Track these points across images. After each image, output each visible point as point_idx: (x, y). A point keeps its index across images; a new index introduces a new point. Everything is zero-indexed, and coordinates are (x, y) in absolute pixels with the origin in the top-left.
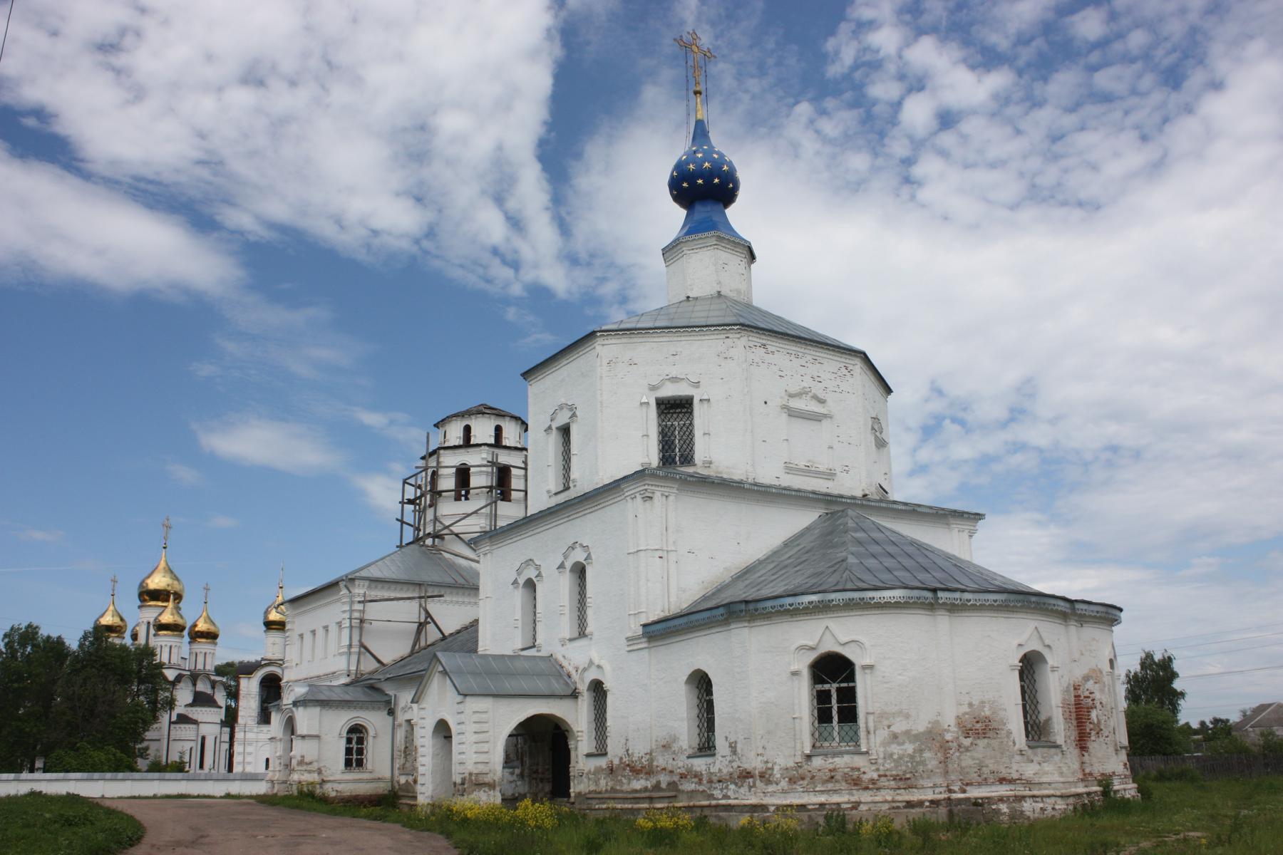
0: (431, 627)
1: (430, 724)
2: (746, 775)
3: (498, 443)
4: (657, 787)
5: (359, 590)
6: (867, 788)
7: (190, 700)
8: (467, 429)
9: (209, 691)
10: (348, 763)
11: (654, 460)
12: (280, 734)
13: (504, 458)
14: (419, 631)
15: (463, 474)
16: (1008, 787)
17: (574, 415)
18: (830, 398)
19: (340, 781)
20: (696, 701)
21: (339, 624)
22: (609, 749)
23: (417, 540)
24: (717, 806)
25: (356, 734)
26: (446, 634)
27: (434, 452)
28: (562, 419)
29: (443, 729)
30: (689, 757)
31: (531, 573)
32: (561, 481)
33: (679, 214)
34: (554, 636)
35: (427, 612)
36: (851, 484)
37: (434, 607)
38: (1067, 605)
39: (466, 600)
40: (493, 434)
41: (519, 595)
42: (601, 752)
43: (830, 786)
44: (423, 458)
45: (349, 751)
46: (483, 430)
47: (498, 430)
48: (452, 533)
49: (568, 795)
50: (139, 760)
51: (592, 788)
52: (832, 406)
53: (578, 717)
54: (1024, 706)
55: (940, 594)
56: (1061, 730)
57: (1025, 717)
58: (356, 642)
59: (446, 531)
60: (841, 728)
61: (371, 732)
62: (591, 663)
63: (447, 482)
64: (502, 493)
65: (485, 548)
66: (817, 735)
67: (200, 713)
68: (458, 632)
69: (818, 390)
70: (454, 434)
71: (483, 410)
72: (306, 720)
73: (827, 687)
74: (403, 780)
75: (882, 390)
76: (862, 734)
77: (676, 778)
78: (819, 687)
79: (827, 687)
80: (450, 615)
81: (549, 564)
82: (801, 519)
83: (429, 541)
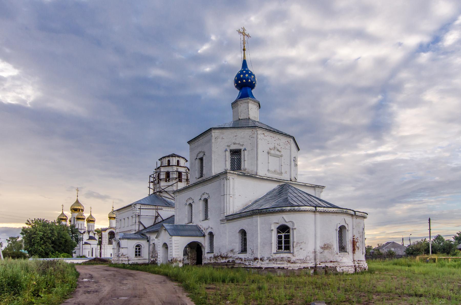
0: (159, 217)
1: (161, 244)
2: (256, 259)
4: (228, 262)
5: (138, 206)
6: (292, 263)
8: (169, 161)
9: (93, 236)
10: (136, 255)
11: (228, 166)
12: (116, 247)
14: (156, 219)
15: (168, 174)
16: (333, 263)
17: (204, 154)
18: (282, 150)
19: (134, 260)
21: (132, 216)
22: (214, 251)
23: (154, 193)
24: (247, 267)
25: (138, 247)
26: (146, 227)
28: (201, 155)
29: (165, 246)
30: (239, 253)
31: (191, 201)
32: (200, 175)
34: (198, 220)
35: (158, 213)
36: (286, 177)
37: (160, 212)
39: (168, 209)
41: (187, 208)
42: (212, 252)
43: (281, 262)
44: (156, 169)
45: (136, 252)
46: (174, 161)
47: (178, 161)
48: (165, 191)
49: (202, 264)
50: (74, 254)
51: (209, 262)
52: (282, 153)
56: (349, 247)
61: (143, 246)
62: (209, 227)
63: (163, 176)
64: (179, 180)
65: (177, 194)
67: (91, 242)
68: (168, 219)
69: (279, 148)
70: (165, 162)
71: (173, 156)
72: (124, 243)
73: (281, 234)
74: (152, 259)
77: (234, 259)
78: (279, 234)
79: (281, 234)
80: (165, 213)
81: (196, 199)
82: (274, 186)
83: (158, 193)
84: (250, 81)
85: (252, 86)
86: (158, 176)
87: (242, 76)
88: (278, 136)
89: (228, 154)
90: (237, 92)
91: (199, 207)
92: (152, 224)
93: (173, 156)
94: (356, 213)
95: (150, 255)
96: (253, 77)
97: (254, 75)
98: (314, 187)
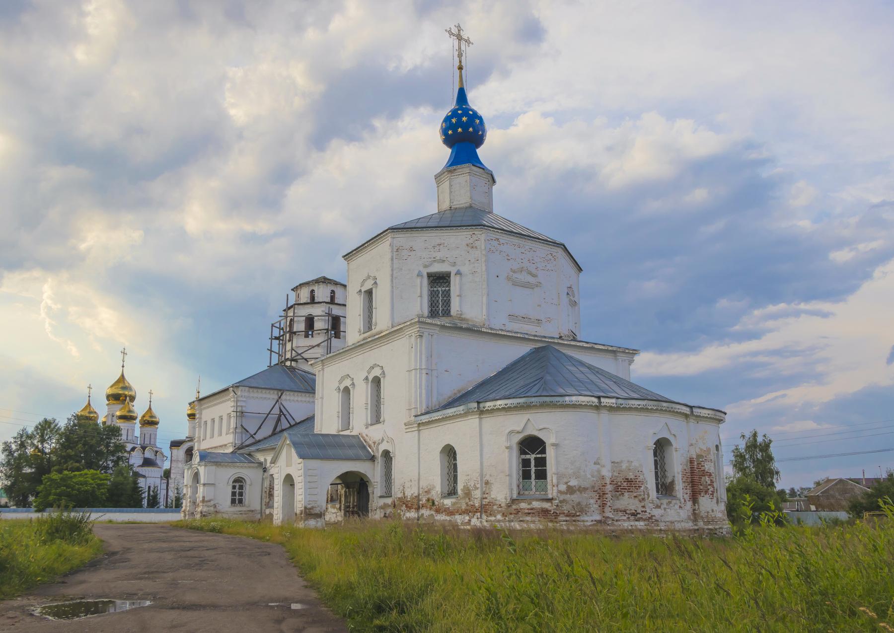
3: (332, 301)
7: (141, 462)
10: (233, 501)
13: (336, 311)
15: (310, 321)
17: (375, 283)
20: (447, 464)
23: (281, 363)
27: (292, 307)
28: (368, 286)
29: (289, 480)
31: (347, 383)
33: (447, 152)
34: (359, 425)
38: (688, 409)
40: (329, 295)
42: (388, 494)
45: (234, 494)
48: (303, 358)
53: (374, 473)
54: (656, 473)
55: (602, 400)
56: (680, 489)
57: (657, 479)
58: (239, 426)
59: (299, 357)
60: (536, 483)
61: (248, 482)
63: (300, 326)
66: (521, 486)
70: (305, 295)
73: (528, 457)
75: (575, 269)
76: (549, 487)
78: (523, 457)
79: (528, 457)
82: (522, 350)
84: (471, 129)
85: (477, 139)
86: (291, 326)
87: (454, 120)
88: (529, 244)
89: (425, 281)
90: (446, 153)
91: (361, 396)
92: (270, 433)
93: (324, 281)
94: (694, 410)
95: (264, 503)
96: (478, 121)
97: (480, 118)
98: (614, 352)
